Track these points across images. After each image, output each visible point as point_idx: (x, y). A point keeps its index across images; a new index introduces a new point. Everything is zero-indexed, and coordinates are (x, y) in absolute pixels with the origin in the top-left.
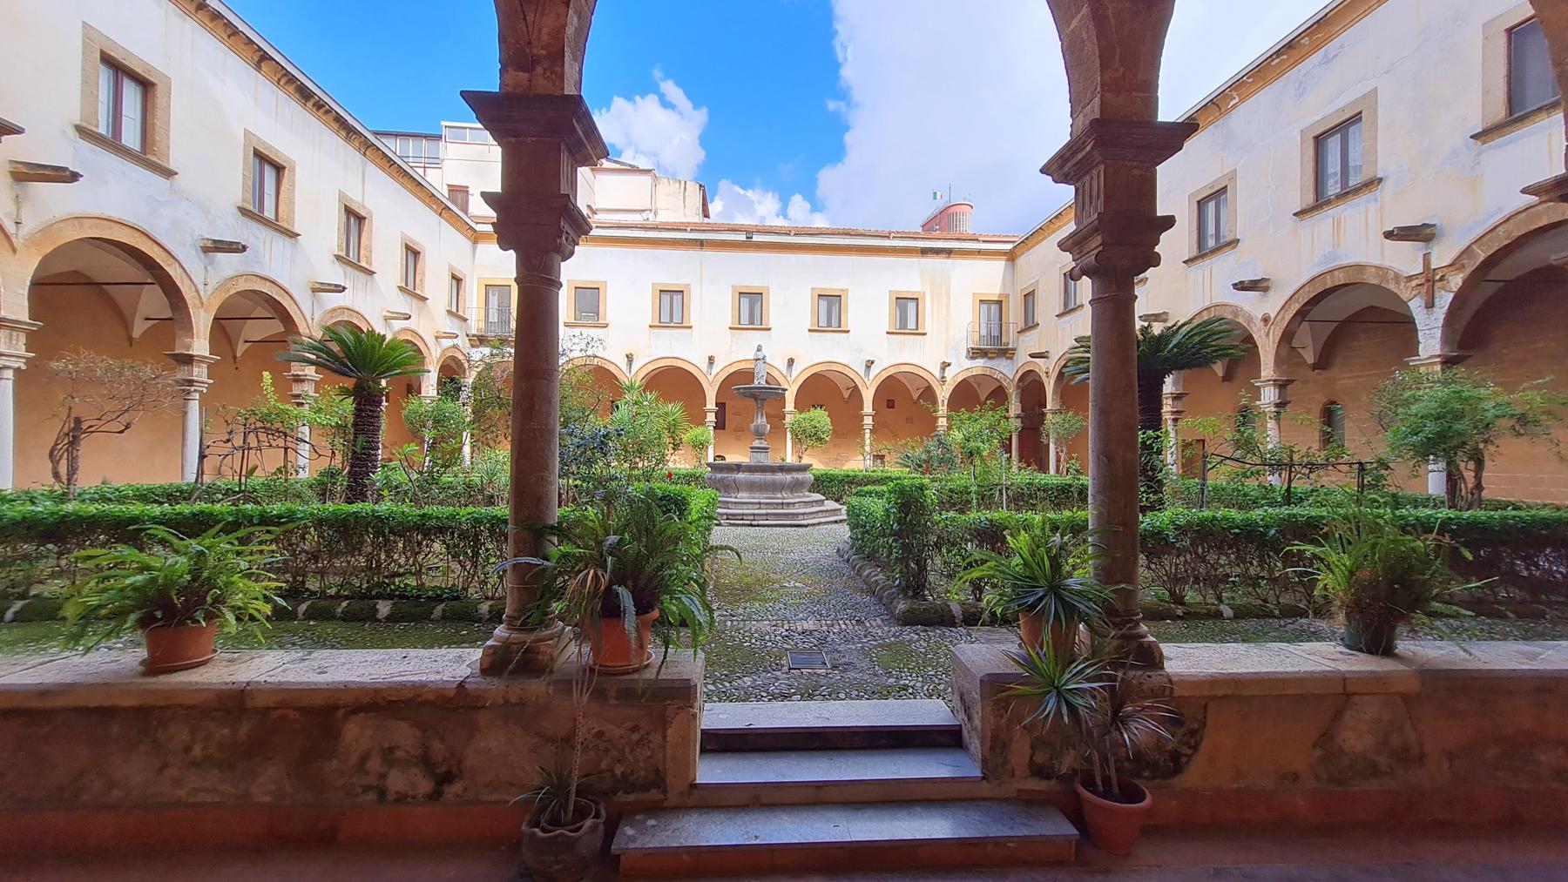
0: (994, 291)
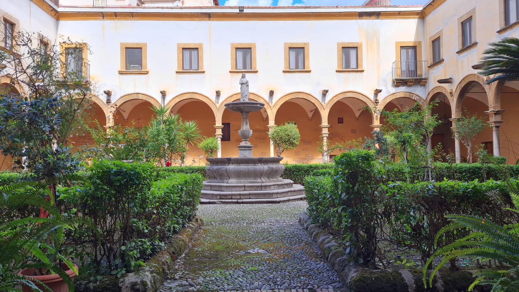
0: (410, 39)
